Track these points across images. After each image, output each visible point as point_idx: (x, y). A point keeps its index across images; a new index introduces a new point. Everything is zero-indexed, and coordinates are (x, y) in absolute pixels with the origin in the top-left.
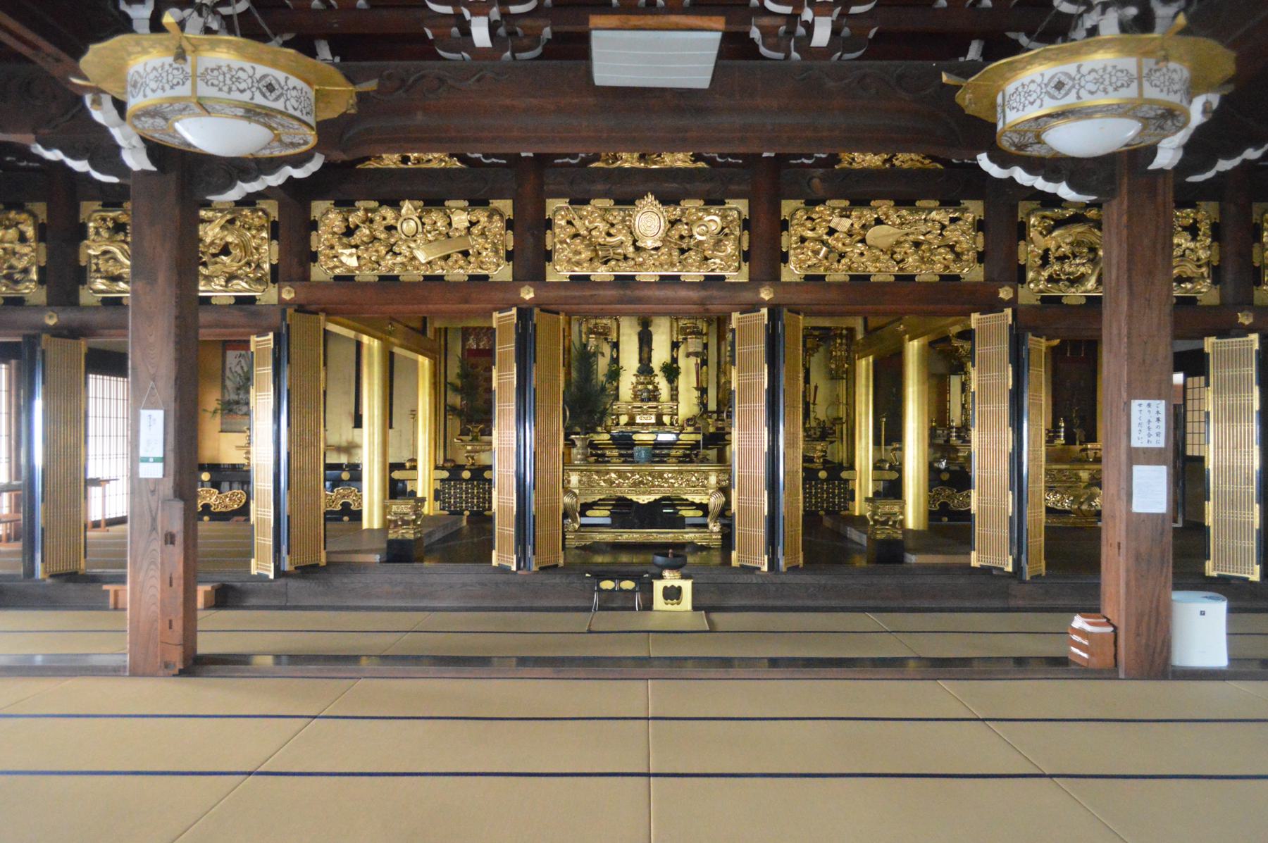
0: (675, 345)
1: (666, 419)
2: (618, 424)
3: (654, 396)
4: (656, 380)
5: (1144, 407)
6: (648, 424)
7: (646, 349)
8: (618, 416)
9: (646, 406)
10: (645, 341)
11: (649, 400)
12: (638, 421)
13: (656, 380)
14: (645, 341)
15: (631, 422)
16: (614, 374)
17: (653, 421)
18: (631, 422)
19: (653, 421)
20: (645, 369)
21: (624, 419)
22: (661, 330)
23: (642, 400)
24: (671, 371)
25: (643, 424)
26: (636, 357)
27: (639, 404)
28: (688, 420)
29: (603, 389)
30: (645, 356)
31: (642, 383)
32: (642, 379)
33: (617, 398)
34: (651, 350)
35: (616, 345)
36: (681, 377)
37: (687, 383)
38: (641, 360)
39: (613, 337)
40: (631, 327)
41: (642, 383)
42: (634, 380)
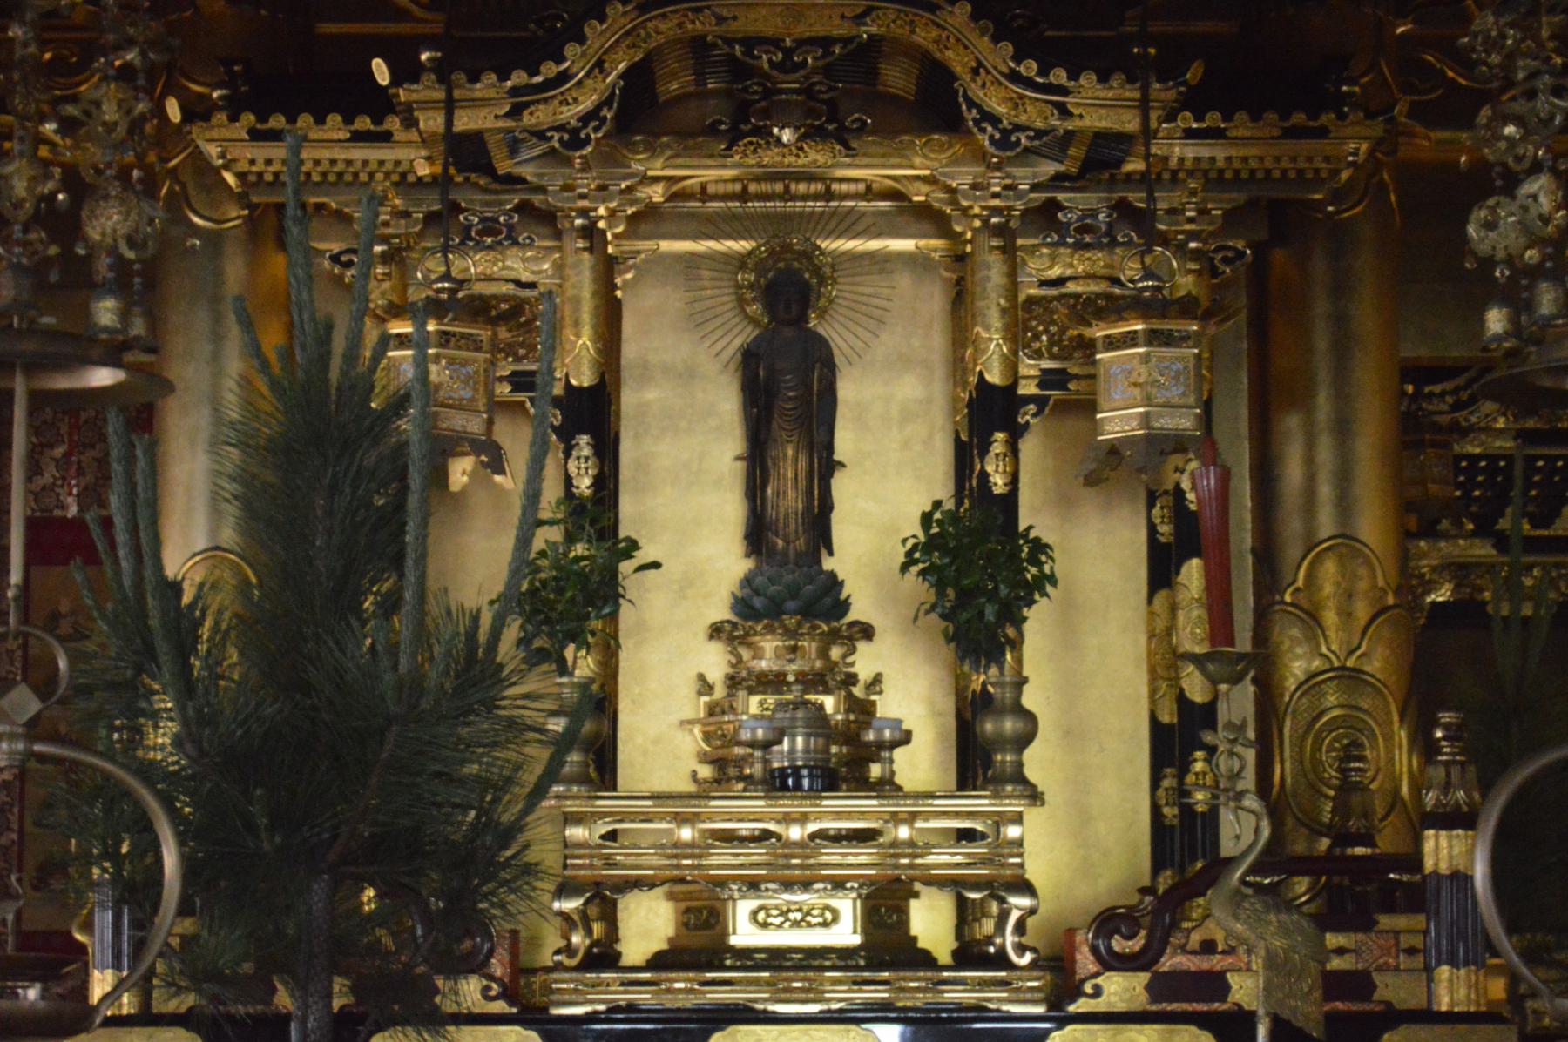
0: (988, 414)
1: (930, 922)
2: (603, 957)
3: (851, 757)
4: (865, 662)
5: (1444, 842)
6: (813, 959)
7: (790, 463)
8: (604, 900)
9: (805, 820)
10: (788, 402)
11: (829, 779)
12: (744, 934)
13: (865, 662)
14: (788, 402)
15: (703, 944)
16: (579, 590)
17: (846, 934)
18: (703, 944)
19: (846, 934)
20: (790, 584)
21: (647, 924)
22: (889, 341)
23: (778, 783)
24: (979, 574)
25: (776, 959)
26: (731, 509)
27: (747, 811)
28: (1108, 922)
29: (477, 673)
30: (788, 499)
31: (770, 682)
32: (768, 653)
33: (602, 765)
34: (825, 466)
35: (592, 414)
36: (1038, 622)
37: (1091, 659)
38: (757, 533)
39: (577, 363)
40: (697, 321)
41: (770, 682)
42: (715, 662)
